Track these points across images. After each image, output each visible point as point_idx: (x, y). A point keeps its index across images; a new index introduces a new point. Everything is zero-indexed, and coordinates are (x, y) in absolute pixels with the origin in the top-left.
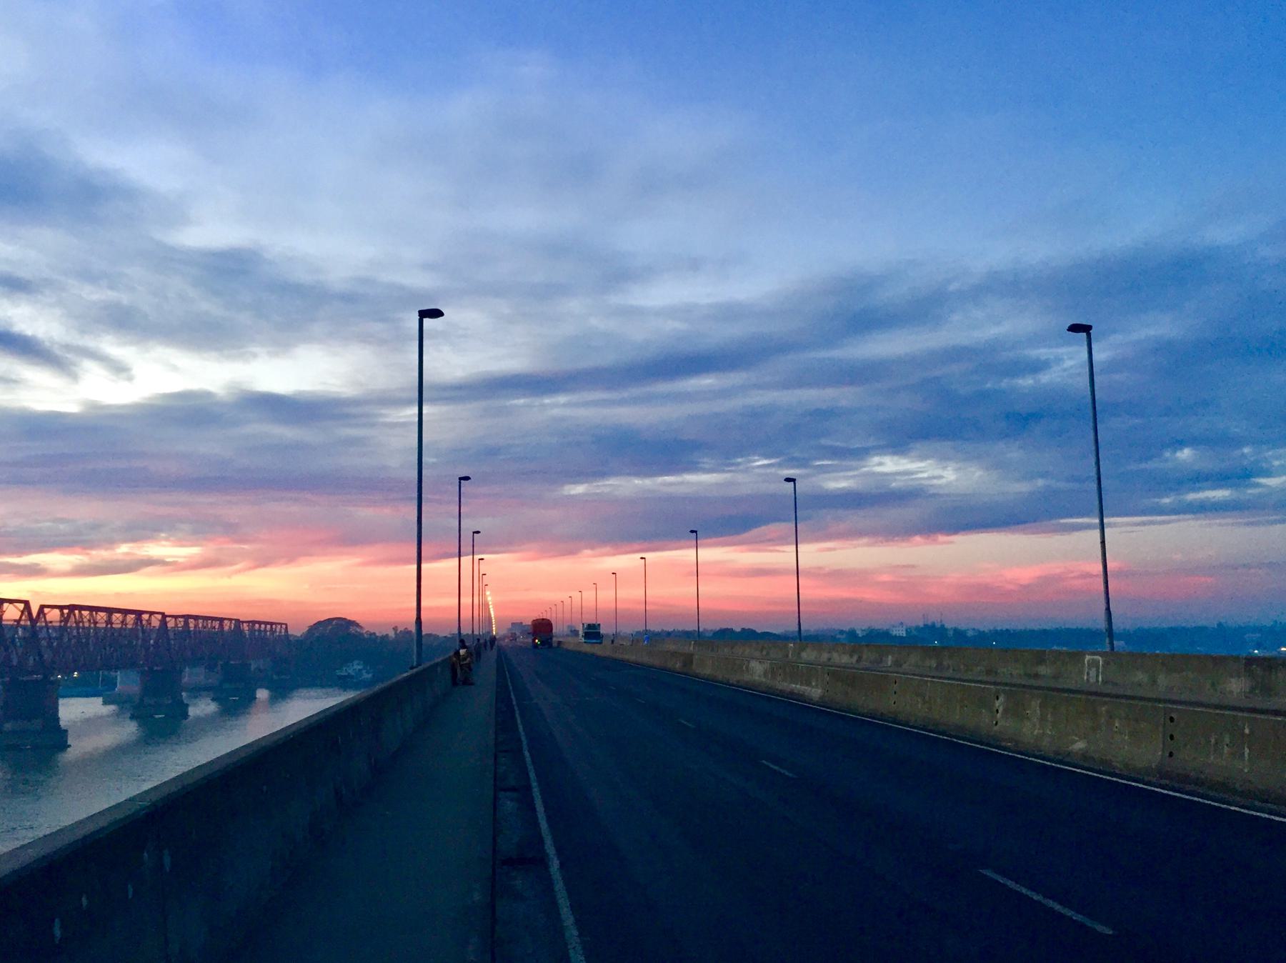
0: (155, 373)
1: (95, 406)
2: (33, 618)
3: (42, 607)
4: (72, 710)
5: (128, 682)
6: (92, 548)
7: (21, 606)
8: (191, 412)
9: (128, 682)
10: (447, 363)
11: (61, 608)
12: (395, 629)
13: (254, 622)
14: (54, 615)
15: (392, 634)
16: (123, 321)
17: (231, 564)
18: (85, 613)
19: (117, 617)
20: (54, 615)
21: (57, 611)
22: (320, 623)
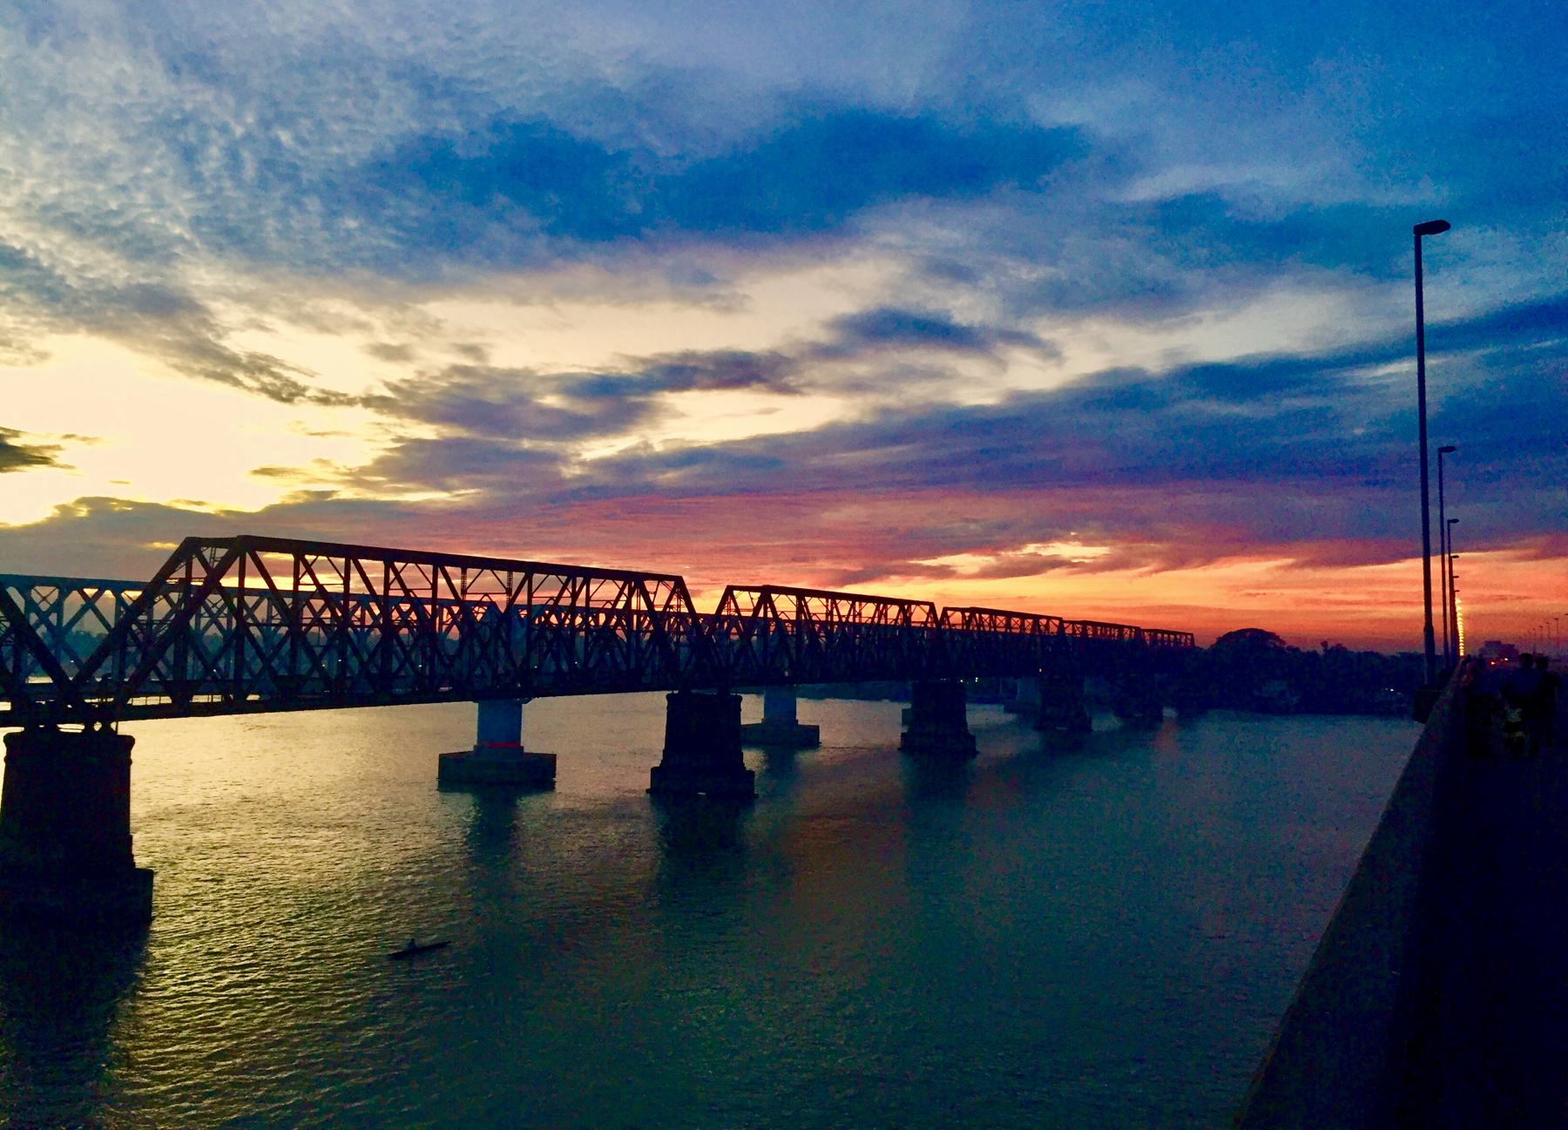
0: (1084, 352)
1: (1018, 396)
2: (938, 620)
3: (945, 610)
4: (979, 716)
5: (1028, 689)
6: (1002, 548)
7: (927, 608)
8: (1121, 394)
9: (1028, 689)
10: (1449, 301)
11: (963, 611)
12: (1324, 644)
13: (1156, 631)
14: (956, 618)
15: (1320, 651)
16: (1064, 299)
17: (1139, 566)
18: (985, 616)
19: (1015, 621)
20: (956, 618)
21: (959, 614)
22: (1230, 634)
